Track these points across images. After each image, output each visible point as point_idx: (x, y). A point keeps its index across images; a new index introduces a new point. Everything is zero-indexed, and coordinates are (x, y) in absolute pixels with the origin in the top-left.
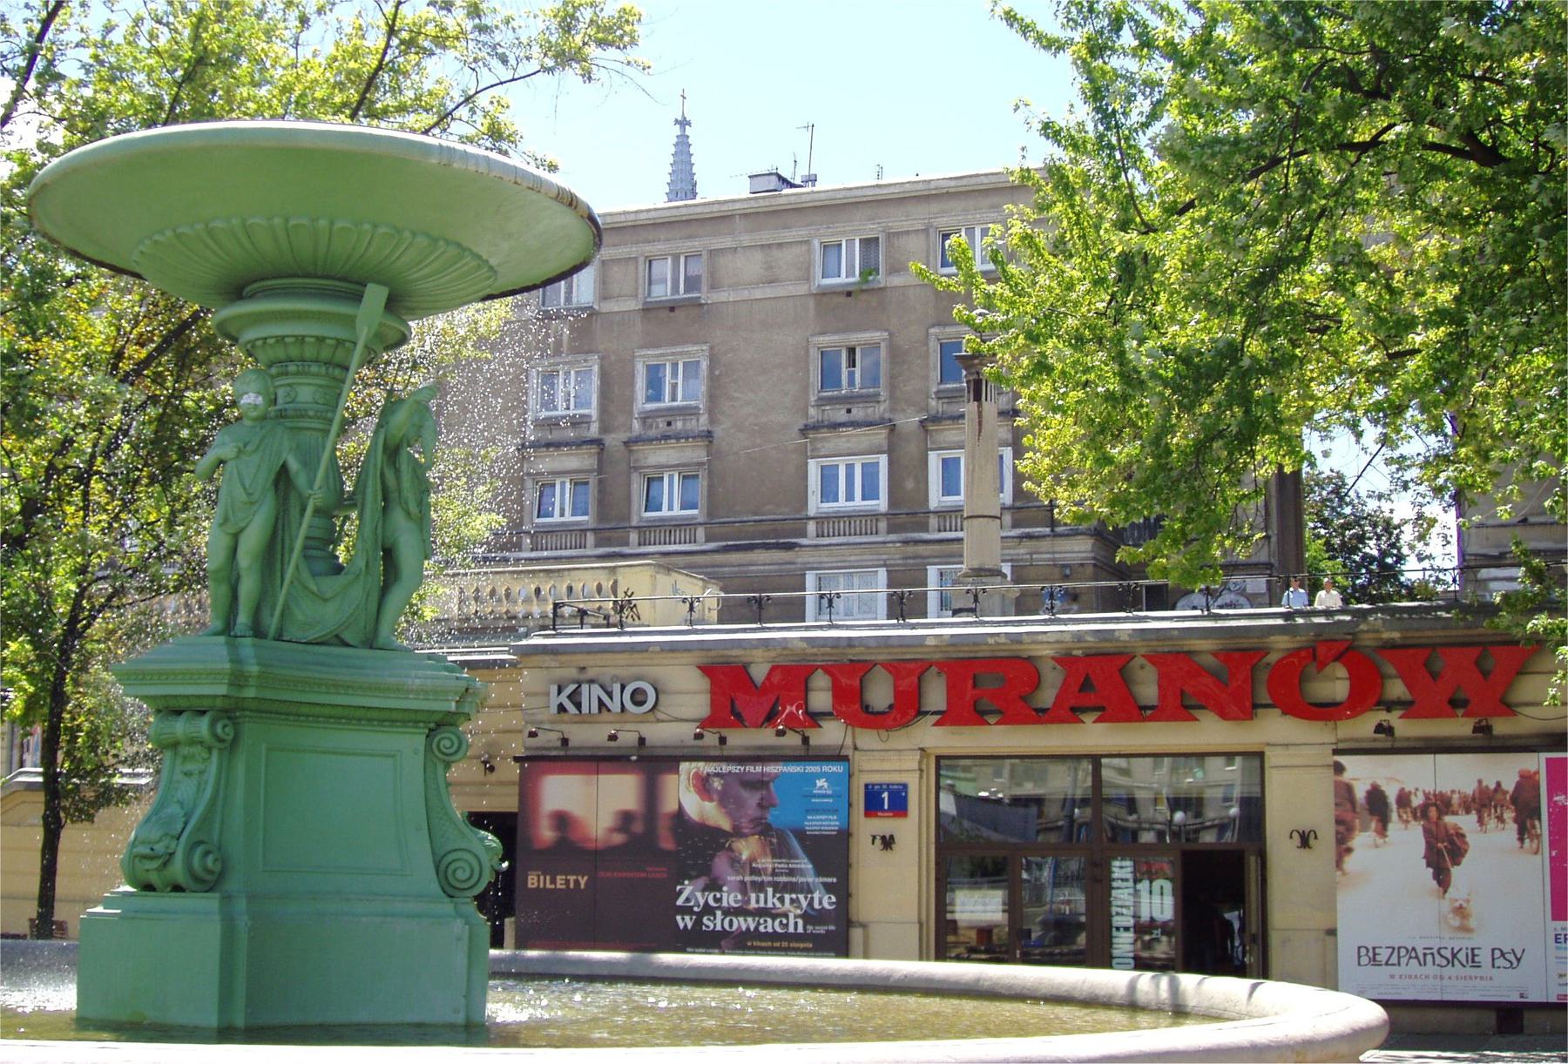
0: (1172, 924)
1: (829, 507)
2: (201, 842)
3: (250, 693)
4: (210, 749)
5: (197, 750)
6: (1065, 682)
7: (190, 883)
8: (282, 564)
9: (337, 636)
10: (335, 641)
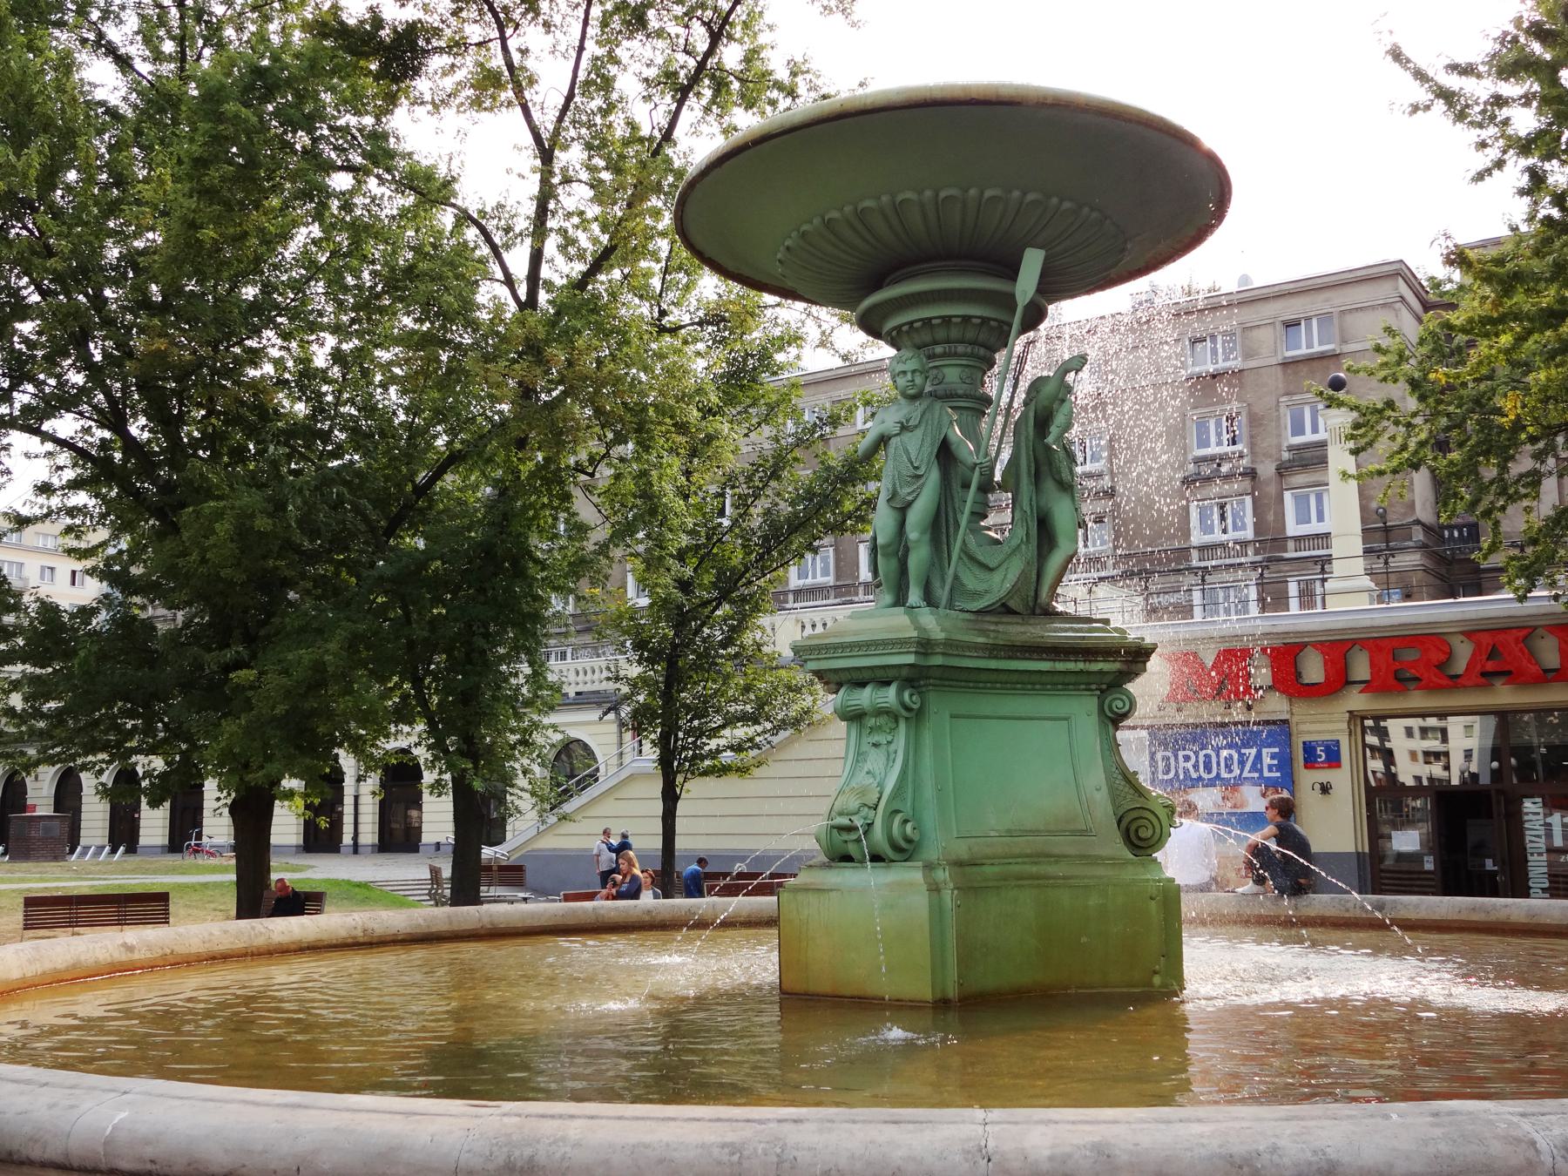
0: (1388, 845)
1: (1208, 539)
2: (897, 812)
3: (937, 660)
4: (896, 718)
5: (882, 720)
6: (1474, 655)
7: (890, 853)
8: (948, 537)
9: (1004, 605)
10: (1003, 609)
